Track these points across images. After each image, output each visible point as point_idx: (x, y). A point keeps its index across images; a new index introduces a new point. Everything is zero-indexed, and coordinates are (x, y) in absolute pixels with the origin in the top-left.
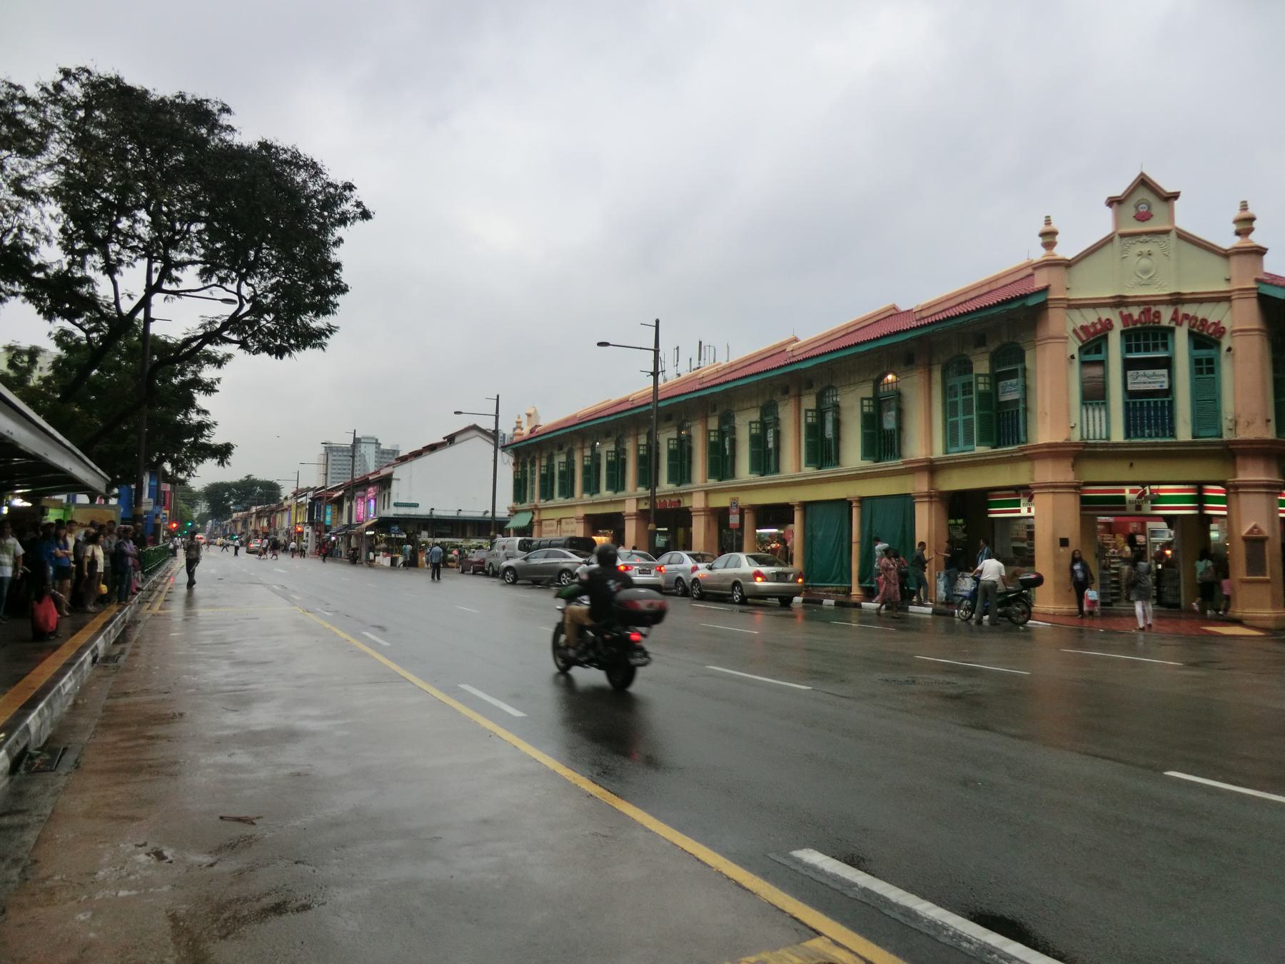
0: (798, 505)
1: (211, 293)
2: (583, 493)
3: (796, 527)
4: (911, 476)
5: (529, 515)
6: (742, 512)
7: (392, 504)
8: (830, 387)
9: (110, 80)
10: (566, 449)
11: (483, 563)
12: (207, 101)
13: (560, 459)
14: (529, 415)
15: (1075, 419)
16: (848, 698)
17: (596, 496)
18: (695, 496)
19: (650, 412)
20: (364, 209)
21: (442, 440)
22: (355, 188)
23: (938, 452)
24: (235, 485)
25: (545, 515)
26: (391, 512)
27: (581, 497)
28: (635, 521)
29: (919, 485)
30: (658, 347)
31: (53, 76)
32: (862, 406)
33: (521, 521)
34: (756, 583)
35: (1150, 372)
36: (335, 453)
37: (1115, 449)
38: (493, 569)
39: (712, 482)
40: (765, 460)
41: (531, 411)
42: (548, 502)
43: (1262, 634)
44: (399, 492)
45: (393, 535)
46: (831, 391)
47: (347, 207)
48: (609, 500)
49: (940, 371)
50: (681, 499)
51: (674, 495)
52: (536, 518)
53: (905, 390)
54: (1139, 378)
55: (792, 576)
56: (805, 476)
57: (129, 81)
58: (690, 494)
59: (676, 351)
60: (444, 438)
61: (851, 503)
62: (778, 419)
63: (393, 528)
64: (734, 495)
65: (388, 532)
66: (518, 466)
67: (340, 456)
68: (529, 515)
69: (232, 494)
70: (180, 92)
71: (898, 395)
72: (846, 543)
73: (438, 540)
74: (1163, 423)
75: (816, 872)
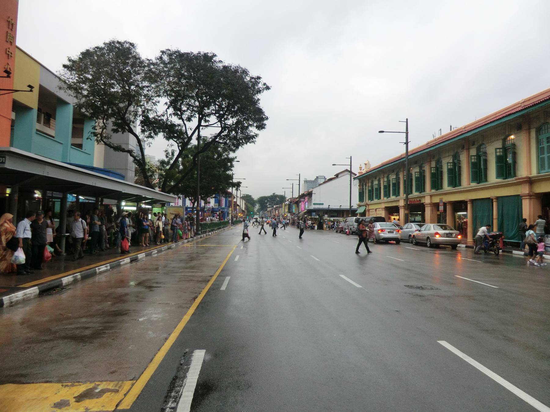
0: (495, 199)
1: (218, 125)
2: (384, 197)
3: (469, 213)
4: (520, 186)
5: (365, 207)
6: (445, 204)
7: (312, 204)
8: (483, 144)
9: (176, 52)
10: (377, 178)
11: (343, 228)
12: (207, 53)
13: (376, 182)
14: (366, 164)
17: (389, 199)
18: (426, 197)
19: (405, 161)
20: (267, 86)
21: (334, 177)
22: (261, 78)
23: (534, 173)
24: (269, 197)
25: (371, 207)
26: (312, 207)
27: (384, 199)
28: (384, 211)
29: (524, 190)
30: (408, 131)
31: (159, 54)
32: (496, 152)
33: (361, 210)
34: (436, 238)
36: (308, 183)
38: (352, 231)
39: (433, 191)
40: (455, 180)
41: (366, 162)
42: (372, 202)
43: (18, 286)
44: (315, 199)
45: (313, 217)
46: (483, 146)
47: (260, 85)
48: (393, 200)
49: (535, 132)
50: (421, 199)
51: (418, 197)
52: (367, 209)
53: (517, 143)
55: (454, 234)
56: (471, 187)
57: (183, 51)
58: (424, 197)
59: (440, 131)
60: (335, 176)
61: (492, 200)
62: (460, 160)
63: (313, 214)
64: (441, 197)
65: (311, 215)
66: (360, 186)
67: (310, 184)
68: (365, 207)
69: (268, 201)
71: (514, 145)
72: (491, 219)
73: (332, 219)
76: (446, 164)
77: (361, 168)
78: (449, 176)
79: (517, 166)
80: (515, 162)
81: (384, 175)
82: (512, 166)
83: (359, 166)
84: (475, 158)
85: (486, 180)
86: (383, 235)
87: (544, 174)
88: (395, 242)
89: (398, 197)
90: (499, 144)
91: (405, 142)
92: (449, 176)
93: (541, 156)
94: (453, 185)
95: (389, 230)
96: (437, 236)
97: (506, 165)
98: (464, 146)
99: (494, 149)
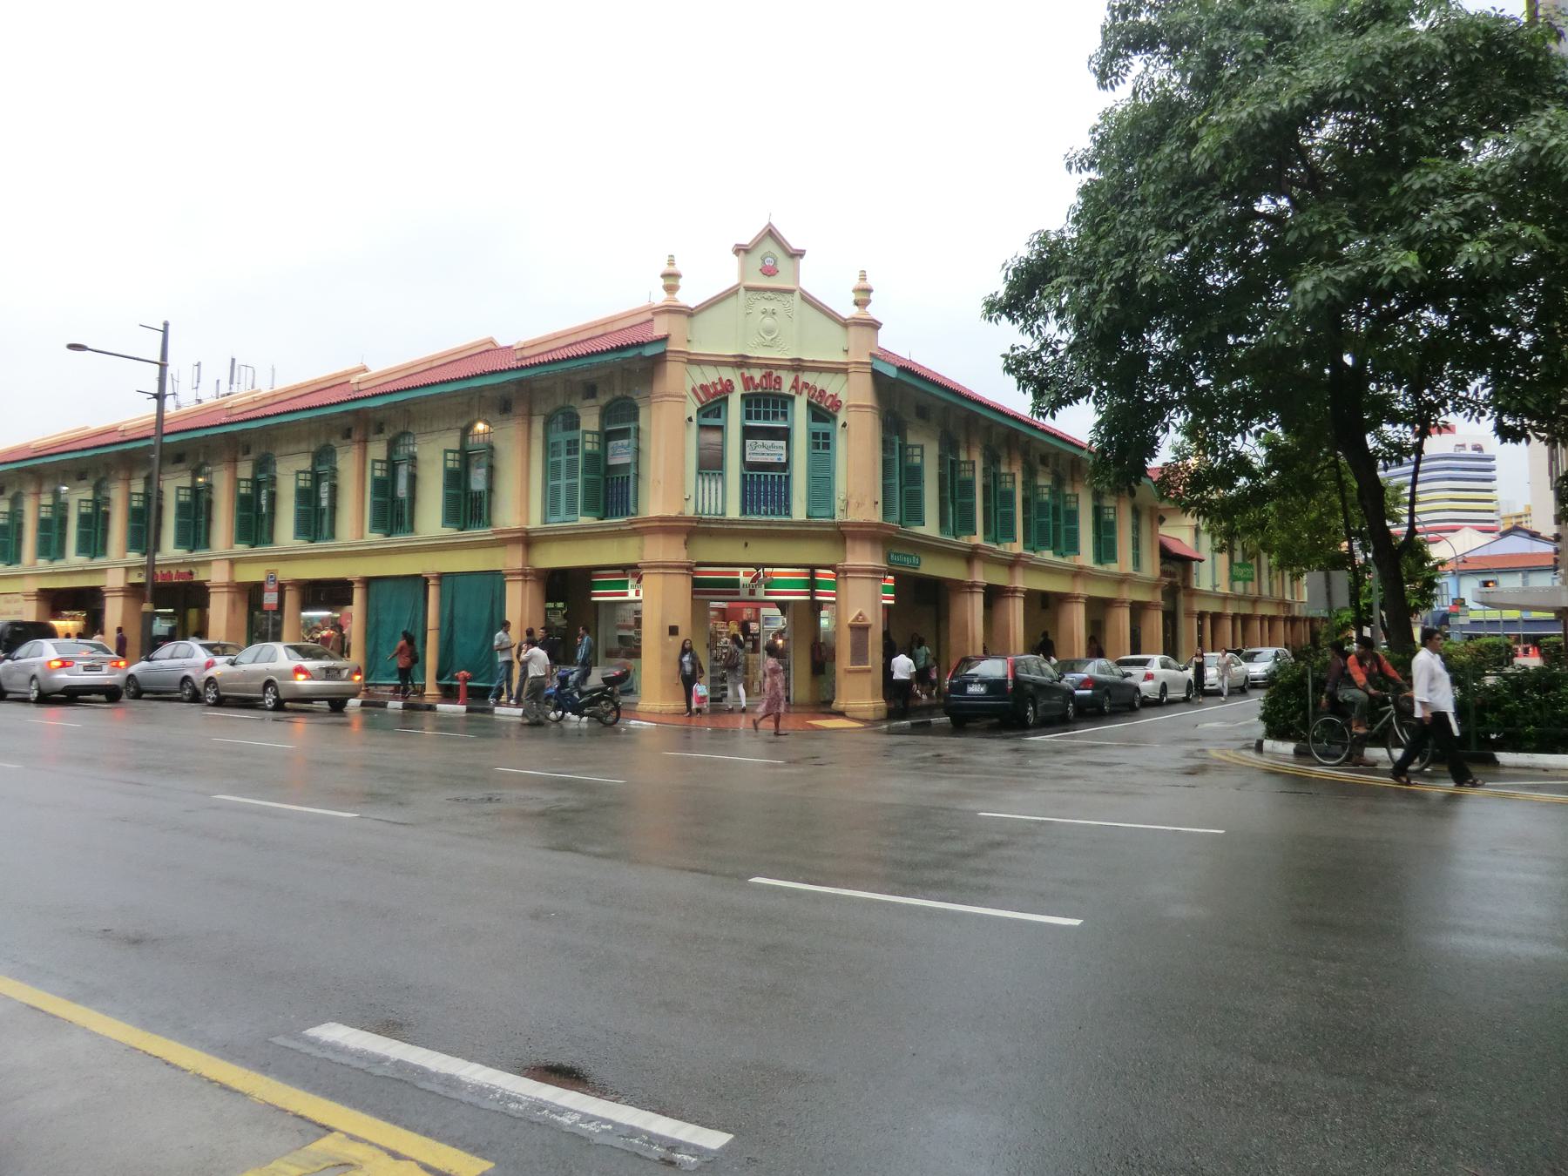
6: (281, 588)
8: (405, 434)
18: (215, 566)
19: (149, 449)
23: (535, 522)
27: (34, 564)
29: (511, 560)
32: (446, 460)
34: (297, 683)
37: (730, 527)
50: (193, 570)
61: (426, 580)
62: (335, 469)
71: (490, 450)
76: (289, 476)
77: (670, 282)
78: (450, 491)
79: (494, 499)
80: (333, 507)
81: (40, 485)
82: (406, 506)
83: (664, 267)
84: (596, 440)
85: (271, 540)
86: (65, 676)
88: (103, 698)
89: (99, 562)
90: (453, 441)
92: (450, 491)
93: (554, 483)
94: (598, 510)
95: (87, 663)
96: (301, 677)
97: (466, 495)
98: (349, 430)
99: (174, 489)
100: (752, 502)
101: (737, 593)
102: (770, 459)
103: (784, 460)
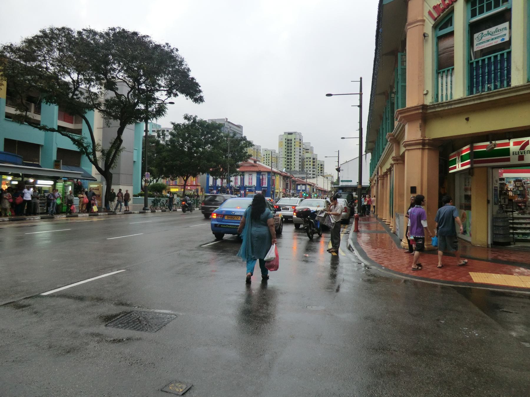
15: (429, 86)
16: (333, 276)
30: (362, 92)
35: (493, 29)
37: (450, 107)
54: (483, 38)
70: (11, 44)
74: (502, 75)
75: (121, 304)
87: (432, 282)
91: (359, 105)
100: (477, 83)
101: (508, 160)
102: (493, 43)
103: (507, 39)
